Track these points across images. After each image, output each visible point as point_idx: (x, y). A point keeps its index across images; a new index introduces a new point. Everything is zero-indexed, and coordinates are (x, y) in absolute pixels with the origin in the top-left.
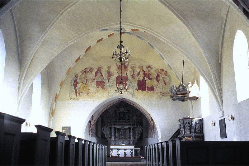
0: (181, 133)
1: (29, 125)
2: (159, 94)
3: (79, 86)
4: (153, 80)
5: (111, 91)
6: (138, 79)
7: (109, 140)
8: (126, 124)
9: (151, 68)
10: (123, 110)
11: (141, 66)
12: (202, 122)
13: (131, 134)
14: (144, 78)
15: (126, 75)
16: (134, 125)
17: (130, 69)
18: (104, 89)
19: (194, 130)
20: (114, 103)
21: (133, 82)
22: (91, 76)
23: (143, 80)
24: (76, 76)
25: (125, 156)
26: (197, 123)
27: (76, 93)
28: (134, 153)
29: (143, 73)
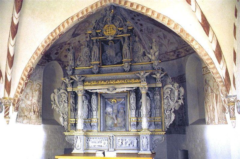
8: (124, 79)
10: (114, 32)
13: (144, 110)
16: (150, 79)
20: (82, 13)
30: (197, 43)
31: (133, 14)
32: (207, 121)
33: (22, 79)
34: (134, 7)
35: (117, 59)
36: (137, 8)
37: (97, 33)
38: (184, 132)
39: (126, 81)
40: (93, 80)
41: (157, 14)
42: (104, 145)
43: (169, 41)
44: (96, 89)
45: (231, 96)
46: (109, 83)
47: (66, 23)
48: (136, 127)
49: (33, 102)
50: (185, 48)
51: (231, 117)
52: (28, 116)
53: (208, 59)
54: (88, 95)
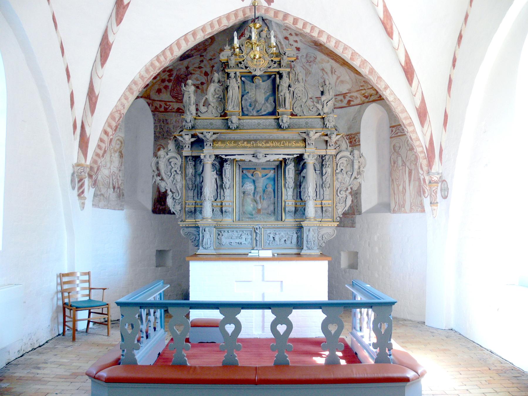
7: (190, 221)
30: (392, 93)
31: (290, 32)
32: (392, 208)
33: (106, 133)
34: (300, 25)
35: (267, 107)
36: (303, 28)
39: (283, 144)
40: (230, 141)
41: (334, 41)
42: (245, 242)
43: (338, 78)
44: (235, 155)
45: (434, 174)
46: (255, 145)
47: (184, 42)
48: (293, 215)
49: (112, 172)
50: (363, 92)
51: (431, 203)
52: (105, 196)
53: (406, 118)
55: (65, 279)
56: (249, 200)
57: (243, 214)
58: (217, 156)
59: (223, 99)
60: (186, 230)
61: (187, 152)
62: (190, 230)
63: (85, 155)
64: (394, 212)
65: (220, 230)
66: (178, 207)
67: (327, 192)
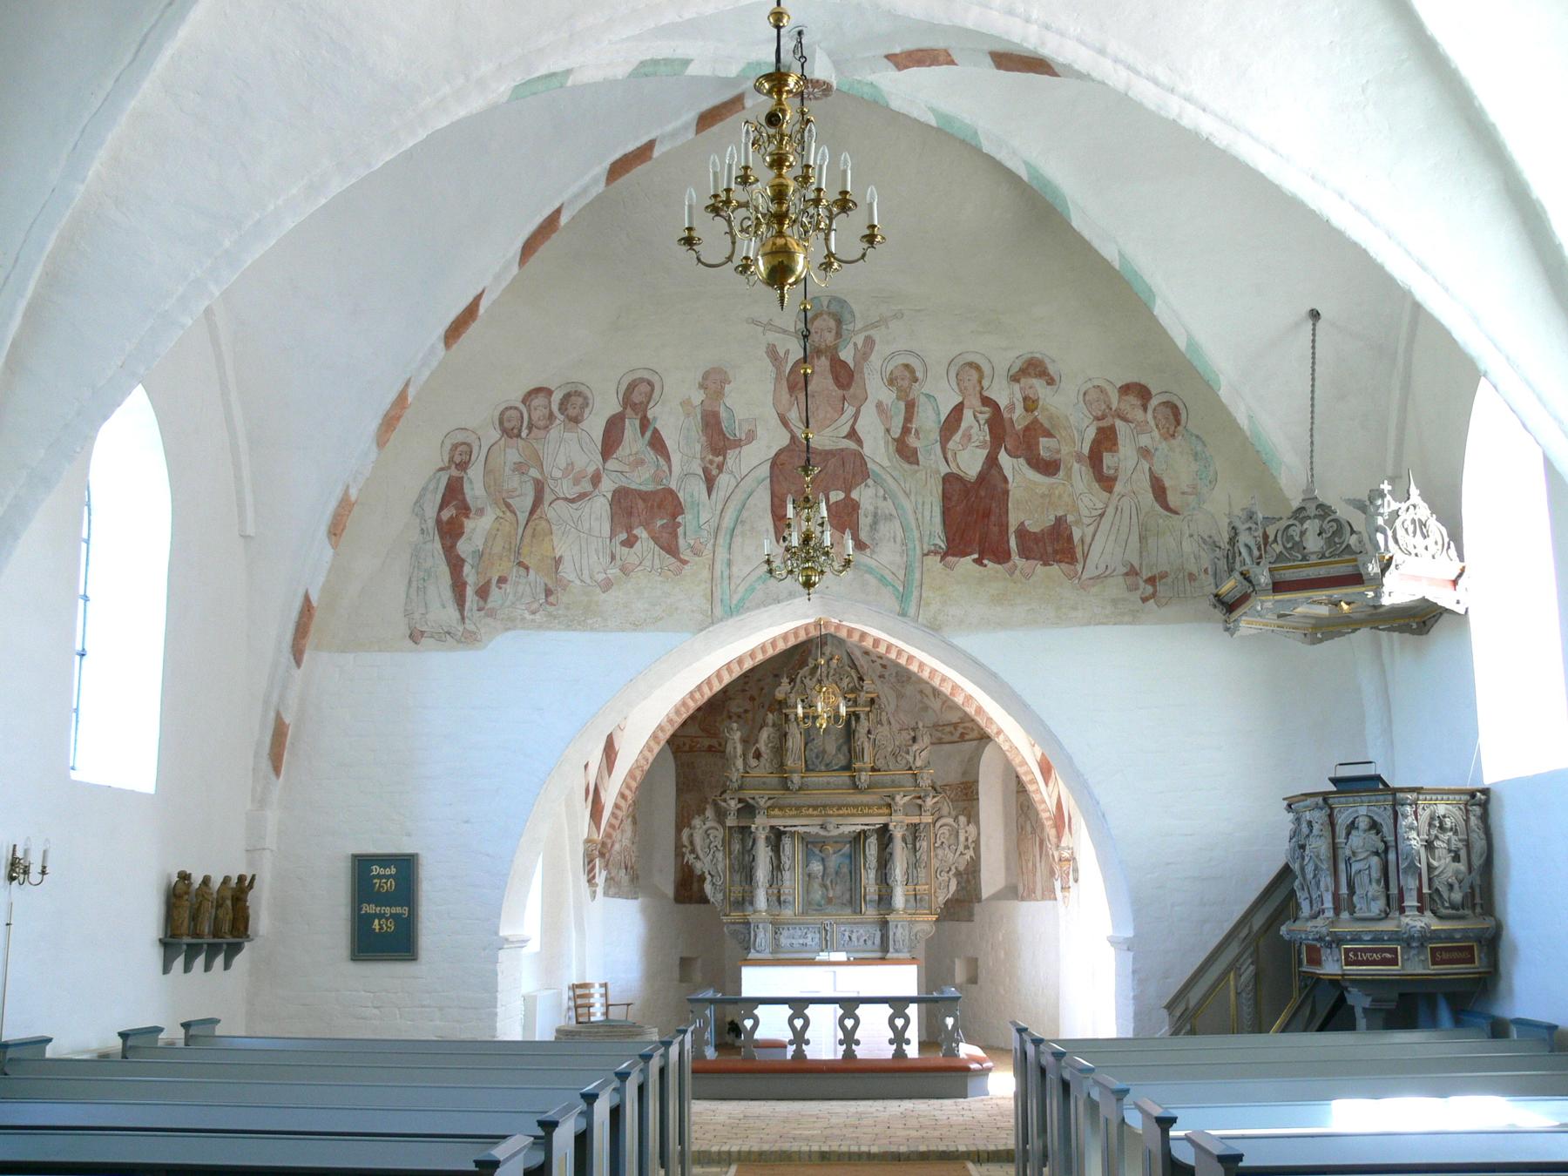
0: (1305, 906)
1: (35, 869)
2: (1116, 586)
3: (478, 530)
4: (1069, 477)
5: (729, 564)
6: (944, 470)
7: (736, 915)
9: (1051, 382)
11: (971, 365)
12: (1485, 818)
14: (992, 461)
15: (853, 434)
17: (877, 390)
18: (671, 549)
19: (1420, 889)
21: (908, 495)
22: (570, 450)
23: (982, 477)
24: (460, 458)
25: (849, 1054)
26: (1441, 828)
27: (459, 588)
28: (912, 1033)
29: (983, 418)
30: (1007, 740)
37: (806, 716)
38: (970, 918)
40: (790, 807)
54: (776, 837)
55: (579, 992)
56: (816, 885)
57: (809, 906)
58: (772, 827)
59: (780, 750)
60: (732, 927)
61: (731, 821)
62: (737, 927)
63: (598, 828)
64: (1023, 899)
65: (777, 926)
66: (720, 896)
67: (922, 873)
